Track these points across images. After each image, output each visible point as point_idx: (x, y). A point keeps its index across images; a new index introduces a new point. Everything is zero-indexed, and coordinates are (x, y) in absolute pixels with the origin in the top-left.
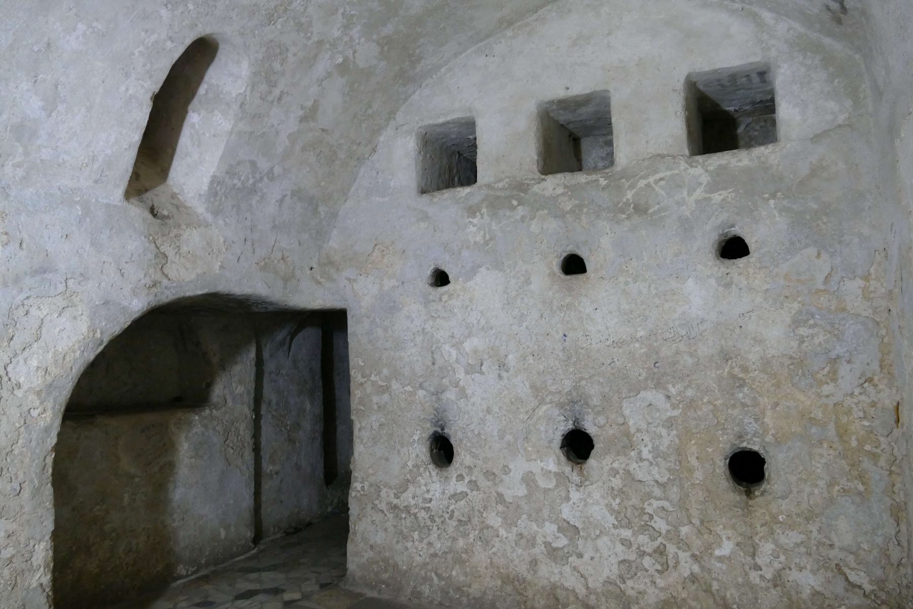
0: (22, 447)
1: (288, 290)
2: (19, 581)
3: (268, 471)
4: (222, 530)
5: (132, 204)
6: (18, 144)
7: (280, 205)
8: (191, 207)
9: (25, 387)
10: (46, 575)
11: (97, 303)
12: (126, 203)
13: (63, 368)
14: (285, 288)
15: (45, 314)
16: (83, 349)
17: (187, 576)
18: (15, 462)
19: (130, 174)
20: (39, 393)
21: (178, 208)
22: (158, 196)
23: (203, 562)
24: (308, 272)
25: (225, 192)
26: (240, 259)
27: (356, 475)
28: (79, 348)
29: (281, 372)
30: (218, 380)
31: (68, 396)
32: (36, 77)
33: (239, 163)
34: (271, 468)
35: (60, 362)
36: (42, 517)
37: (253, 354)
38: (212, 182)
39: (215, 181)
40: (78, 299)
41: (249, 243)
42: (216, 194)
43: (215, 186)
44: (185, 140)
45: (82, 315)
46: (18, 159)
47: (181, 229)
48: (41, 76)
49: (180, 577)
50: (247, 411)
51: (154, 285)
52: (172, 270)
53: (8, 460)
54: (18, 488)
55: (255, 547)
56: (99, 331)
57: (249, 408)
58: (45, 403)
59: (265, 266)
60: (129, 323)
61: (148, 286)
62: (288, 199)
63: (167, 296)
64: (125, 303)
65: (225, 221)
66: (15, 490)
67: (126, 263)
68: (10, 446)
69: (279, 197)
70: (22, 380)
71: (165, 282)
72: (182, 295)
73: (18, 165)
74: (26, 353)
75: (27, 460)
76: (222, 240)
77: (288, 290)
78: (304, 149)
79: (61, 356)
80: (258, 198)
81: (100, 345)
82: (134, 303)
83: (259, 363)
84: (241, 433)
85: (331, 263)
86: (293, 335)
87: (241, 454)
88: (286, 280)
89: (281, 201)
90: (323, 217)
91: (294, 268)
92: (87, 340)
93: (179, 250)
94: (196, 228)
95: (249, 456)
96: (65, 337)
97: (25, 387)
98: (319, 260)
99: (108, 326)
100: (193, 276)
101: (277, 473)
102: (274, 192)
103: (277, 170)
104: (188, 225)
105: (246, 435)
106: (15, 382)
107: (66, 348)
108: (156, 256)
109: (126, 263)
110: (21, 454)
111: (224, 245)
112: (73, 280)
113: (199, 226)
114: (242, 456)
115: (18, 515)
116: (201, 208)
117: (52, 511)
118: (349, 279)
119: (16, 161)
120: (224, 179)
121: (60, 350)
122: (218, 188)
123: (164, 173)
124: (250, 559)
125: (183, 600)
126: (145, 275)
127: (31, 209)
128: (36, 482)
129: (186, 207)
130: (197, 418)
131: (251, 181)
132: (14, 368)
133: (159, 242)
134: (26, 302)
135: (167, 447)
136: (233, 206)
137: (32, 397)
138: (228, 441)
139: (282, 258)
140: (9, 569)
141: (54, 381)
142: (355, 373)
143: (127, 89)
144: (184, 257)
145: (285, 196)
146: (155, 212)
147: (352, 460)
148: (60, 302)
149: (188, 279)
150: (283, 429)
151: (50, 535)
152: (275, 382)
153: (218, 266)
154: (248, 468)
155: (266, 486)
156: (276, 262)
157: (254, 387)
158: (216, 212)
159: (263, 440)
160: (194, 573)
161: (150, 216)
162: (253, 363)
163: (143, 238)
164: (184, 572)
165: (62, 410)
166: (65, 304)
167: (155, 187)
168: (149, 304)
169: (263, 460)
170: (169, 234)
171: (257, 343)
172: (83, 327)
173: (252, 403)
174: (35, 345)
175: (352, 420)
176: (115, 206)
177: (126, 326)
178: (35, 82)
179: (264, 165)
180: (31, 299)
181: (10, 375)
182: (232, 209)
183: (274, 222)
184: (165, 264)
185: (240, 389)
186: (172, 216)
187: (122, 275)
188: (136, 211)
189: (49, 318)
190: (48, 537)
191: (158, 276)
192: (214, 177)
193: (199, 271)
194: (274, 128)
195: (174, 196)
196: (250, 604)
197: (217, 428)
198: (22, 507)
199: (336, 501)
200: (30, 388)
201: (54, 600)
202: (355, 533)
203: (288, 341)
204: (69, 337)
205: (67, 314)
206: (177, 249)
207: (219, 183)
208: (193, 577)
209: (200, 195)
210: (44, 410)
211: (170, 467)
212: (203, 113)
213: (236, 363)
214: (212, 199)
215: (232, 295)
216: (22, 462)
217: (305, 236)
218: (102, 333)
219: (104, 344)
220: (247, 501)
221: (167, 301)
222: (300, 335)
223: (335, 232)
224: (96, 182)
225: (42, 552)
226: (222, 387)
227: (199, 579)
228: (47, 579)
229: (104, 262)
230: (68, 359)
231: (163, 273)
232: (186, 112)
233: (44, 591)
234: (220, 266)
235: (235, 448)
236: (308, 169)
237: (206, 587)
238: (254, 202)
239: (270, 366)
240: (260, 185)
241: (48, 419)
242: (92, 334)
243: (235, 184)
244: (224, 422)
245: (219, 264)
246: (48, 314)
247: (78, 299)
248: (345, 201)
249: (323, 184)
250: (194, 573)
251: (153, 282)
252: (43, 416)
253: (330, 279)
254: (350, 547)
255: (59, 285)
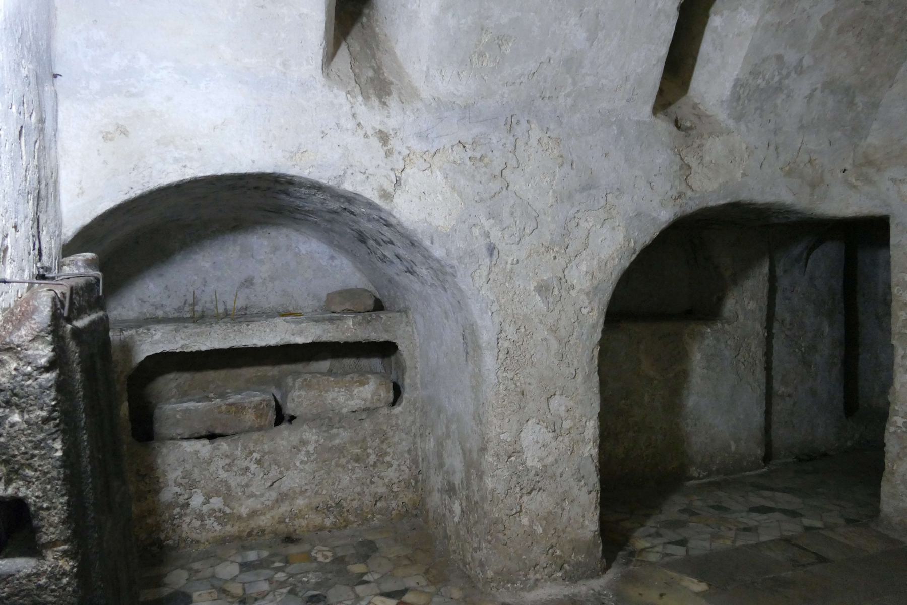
0: (577, 339)
1: (816, 197)
2: (576, 449)
3: (780, 392)
4: (732, 443)
5: (659, 118)
6: (568, 76)
7: (808, 102)
8: (712, 116)
9: (578, 288)
10: (594, 448)
11: (631, 215)
12: (653, 119)
13: (605, 273)
14: (812, 194)
15: (591, 225)
16: (620, 257)
17: (699, 479)
18: (572, 350)
19: (657, 89)
20: (587, 294)
21: (700, 118)
22: (681, 108)
23: (714, 469)
24: (840, 175)
25: (748, 94)
26: (763, 166)
27: (897, 408)
28: (617, 256)
29: (796, 289)
30: (730, 295)
31: (609, 298)
32: (582, 10)
33: (764, 61)
34: (782, 389)
35: (603, 267)
36: (591, 399)
37: (766, 269)
38: (735, 86)
39: (738, 84)
40: (615, 212)
41: (772, 148)
42: (739, 98)
43: (738, 89)
44: (706, 47)
45: (619, 226)
46: (568, 90)
47: (704, 139)
48: (586, 8)
49: (693, 478)
50: (759, 327)
51: (680, 196)
52: (695, 181)
53: (567, 349)
54: (574, 373)
55: (765, 466)
56: (633, 241)
57: (761, 325)
58: (592, 303)
59: (790, 172)
60: (658, 233)
61: (674, 197)
62: (818, 94)
63: (692, 206)
64: (654, 215)
65: (747, 126)
66: (572, 373)
67: (655, 176)
68: (567, 338)
69: (808, 92)
70: (575, 282)
71: (689, 193)
72: (704, 205)
73: (568, 95)
74: (578, 258)
75: (580, 350)
76: (744, 146)
77: (816, 197)
78: (840, 31)
79: (604, 263)
80: (784, 97)
81: (634, 253)
82: (662, 214)
83: (773, 279)
84: (753, 349)
85: (869, 163)
86: (811, 250)
87: (752, 370)
88: (813, 186)
89: (810, 97)
90: (860, 109)
91: (823, 172)
92: (624, 249)
93: (702, 160)
94: (718, 137)
95: (761, 375)
96: (606, 246)
97: (578, 288)
98: (854, 161)
99: (640, 236)
100: (715, 186)
101: (789, 396)
102: (802, 87)
103: (807, 62)
104: (711, 134)
105: (758, 352)
106: (570, 284)
107: (607, 256)
108: (681, 168)
109: (655, 176)
110: (575, 344)
111: (747, 152)
112: (611, 194)
113: (721, 134)
114: (753, 372)
115: (574, 395)
116: (722, 116)
117: (598, 396)
118: (894, 181)
119: (567, 92)
120: (747, 80)
121: (603, 257)
122: (741, 92)
123: (685, 85)
124: (761, 476)
125: (698, 499)
126: (671, 187)
127: (578, 132)
128: (587, 370)
129: (708, 117)
130: (709, 330)
131: (777, 79)
132: (569, 272)
133: (683, 154)
134: (577, 215)
135: (682, 356)
136: (756, 109)
137: (583, 297)
138: (739, 357)
139: (810, 161)
140: (569, 437)
141: (599, 284)
142: (899, 291)
143: (656, 4)
144: (706, 167)
145: (814, 90)
146: (679, 125)
147: (891, 391)
148: (602, 215)
149: (711, 189)
150: (797, 350)
151: (597, 416)
152: (789, 299)
153: (740, 174)
154: (759, 386)
155: (778, 406)
156: (802, 165)
157: (767, 303)
158: (739, 118)
159: (775, 363)
160: (704, 477)
161: (675, 129)
162: (766, 278)
163: (669, 151)
164: (696, 475)
165: (605, 310)
166: (605, 216)
167: (677, 100)
168: (675, 215)
169: (774, 380)
170: (692, 145)
171: (770, 261)
172: (620, 236)
173: (764, 318)
174: (584, 253)
175: (893, 346)
176: (645, 123)
177: (655, 236)
178: (581, 16)
179: (791, 57)
180: (581, 212)
181: (567, 278)
182: (755, 113)
183: (801, 121)
184: (689, 175)
185: (752, 305)
186: (696, 126)
187: (652, 188)
188: (663, 125)
189: (594, 229)
190: (595, 417)
191: (683, 187)
192: (737, 80)
193: (721, 180)
194: (805, 12)
195: (695, 106)
196: (765, 520)
197: (729, 343)
198: (577, 389)
199: (857, 436)
200: (581, 289)
201: (600, 470)
202: (893, 473)
203: (805, 255)
204: (609, 246)
205: (607, 225)
206: (700, 159)
207: (742, 85)
208: (704, 481)
209: (722, 101)
210: (592, 309)
211: (683, 376)
212: (726, 13)
213: (748, 278)
214: (734, 104)
215: (754, 204)
216: (577, 352)
217: (838, 134)
218: (635, 243)
219: (637, 253)
220: (758, 419)
221: (691, 212)
222: (818, 253)
223: (875, 126)
224: (628, 101)
225: (591, 429)
226: (733, 301)
227: (710, 484)
228: (595, 451)
229: (636, 177)
230: (608, 265)
231: (688, 184)
232: (708, 17)
233: (593, 461)
234: (742, 174)
235: (746, 363)
236: (844, 54)
237: (720, 493)
238: (779, 102)
239: (783, 282)
240: (786, 82)
241: (594, 317)
242: (627, 243)
243: (759, 85)
244: (736, 336)
245: (742, 172)
246: (593, 225)
247: (615, 212)
248: (891, 87)
249: (862, 69)
250: (704, 477)
251: (679, 193)
252: (591, 314)
253: (868, 180)
254: (885, 488)
255: (600, 198)
